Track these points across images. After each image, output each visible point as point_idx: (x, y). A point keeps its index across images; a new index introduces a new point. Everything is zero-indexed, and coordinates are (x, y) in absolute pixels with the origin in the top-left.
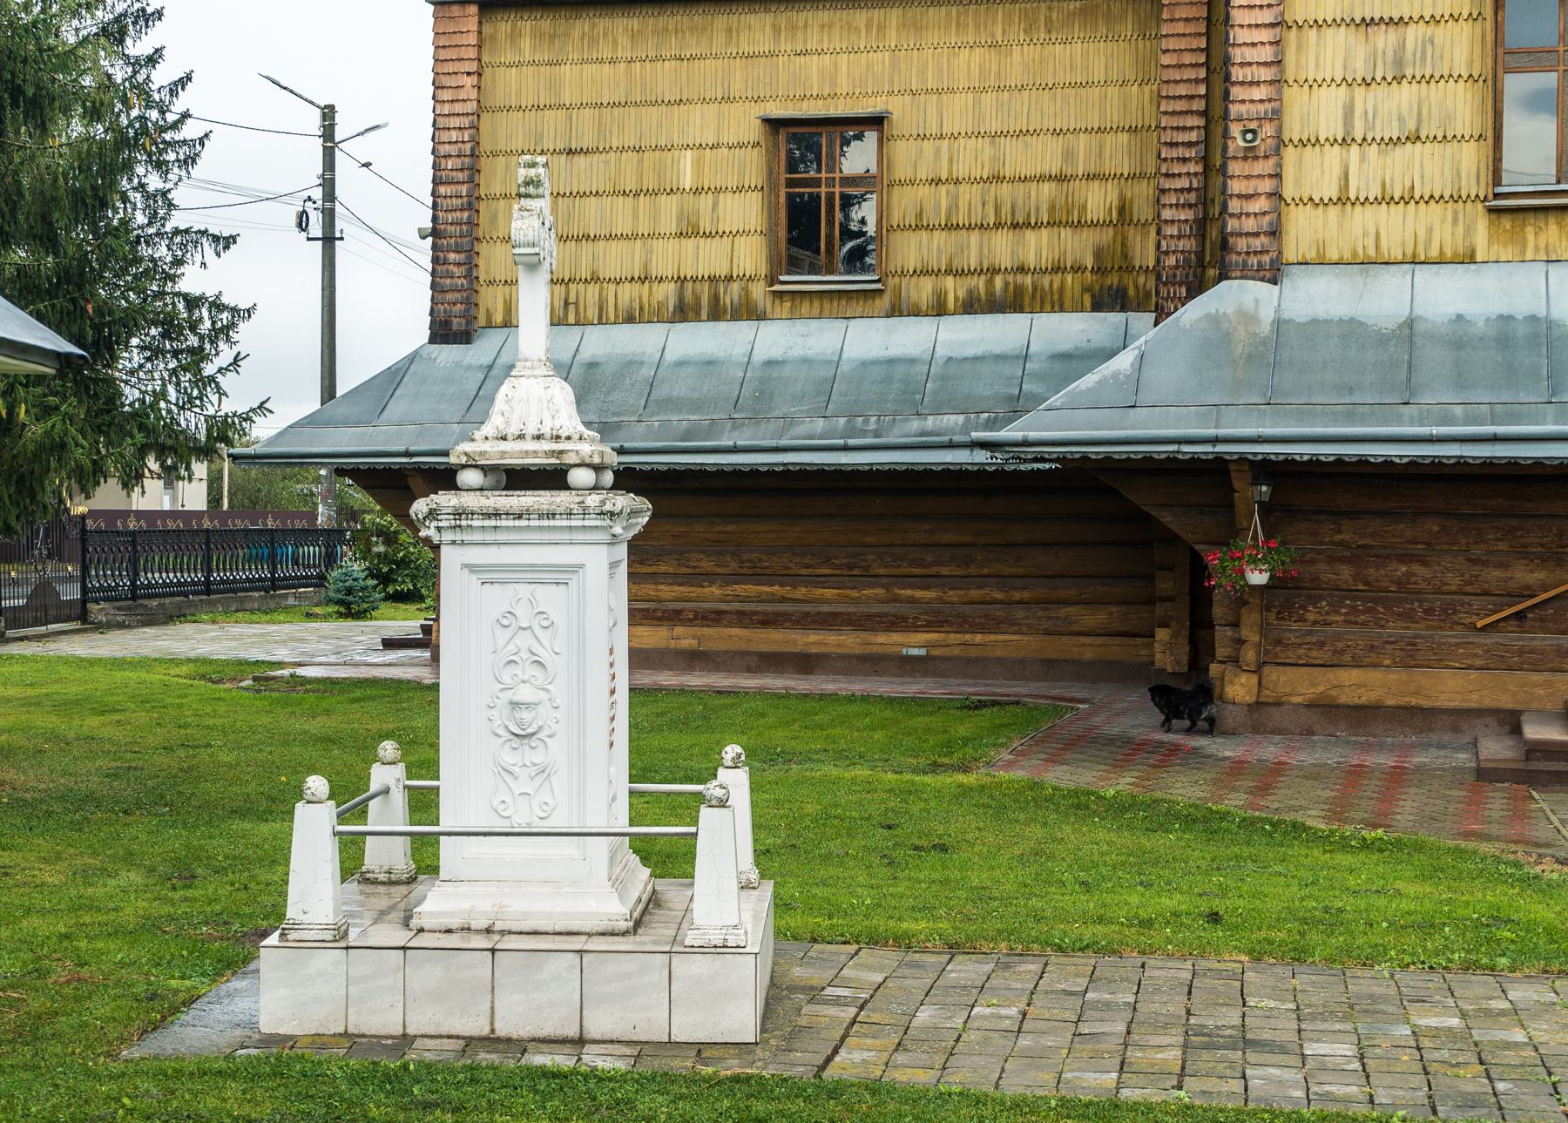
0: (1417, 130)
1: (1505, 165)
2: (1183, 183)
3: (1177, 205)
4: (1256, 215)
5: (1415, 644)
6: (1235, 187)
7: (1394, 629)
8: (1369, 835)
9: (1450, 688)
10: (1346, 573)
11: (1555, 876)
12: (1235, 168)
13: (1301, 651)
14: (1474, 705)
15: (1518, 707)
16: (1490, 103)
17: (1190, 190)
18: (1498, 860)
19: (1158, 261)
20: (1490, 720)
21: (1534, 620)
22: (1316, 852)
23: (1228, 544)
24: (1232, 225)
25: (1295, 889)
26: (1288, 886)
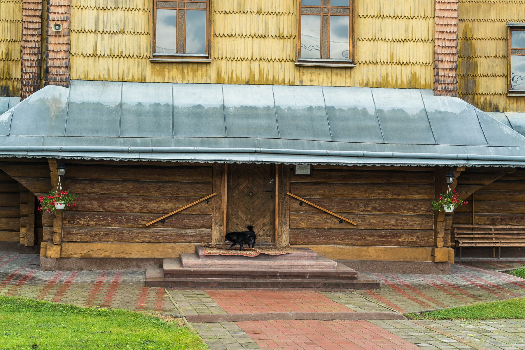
0: (124, 29)
1: (157, 45)
2: (32, 45)
3: (30, 54)
4: (60, 59)
5: (123, 233)
6: (51, 47)
7: (115, 227)
8: (101, 310)
9: (136, 250)
10: (96, 204)
11: (171, 323)
12: (51, 40)
13: (78, 236)
14: (145, 257)
15: (162, 257)
16: (151, 20)
17: (35, 48)
18: (150, 317)
19: (22, 76)
20: (152, 262)
21: (168, 223)
22: (80, 318)
23: (48, 193)
24: (50, 63)
25: (69, 333)
26: (67, 332)
